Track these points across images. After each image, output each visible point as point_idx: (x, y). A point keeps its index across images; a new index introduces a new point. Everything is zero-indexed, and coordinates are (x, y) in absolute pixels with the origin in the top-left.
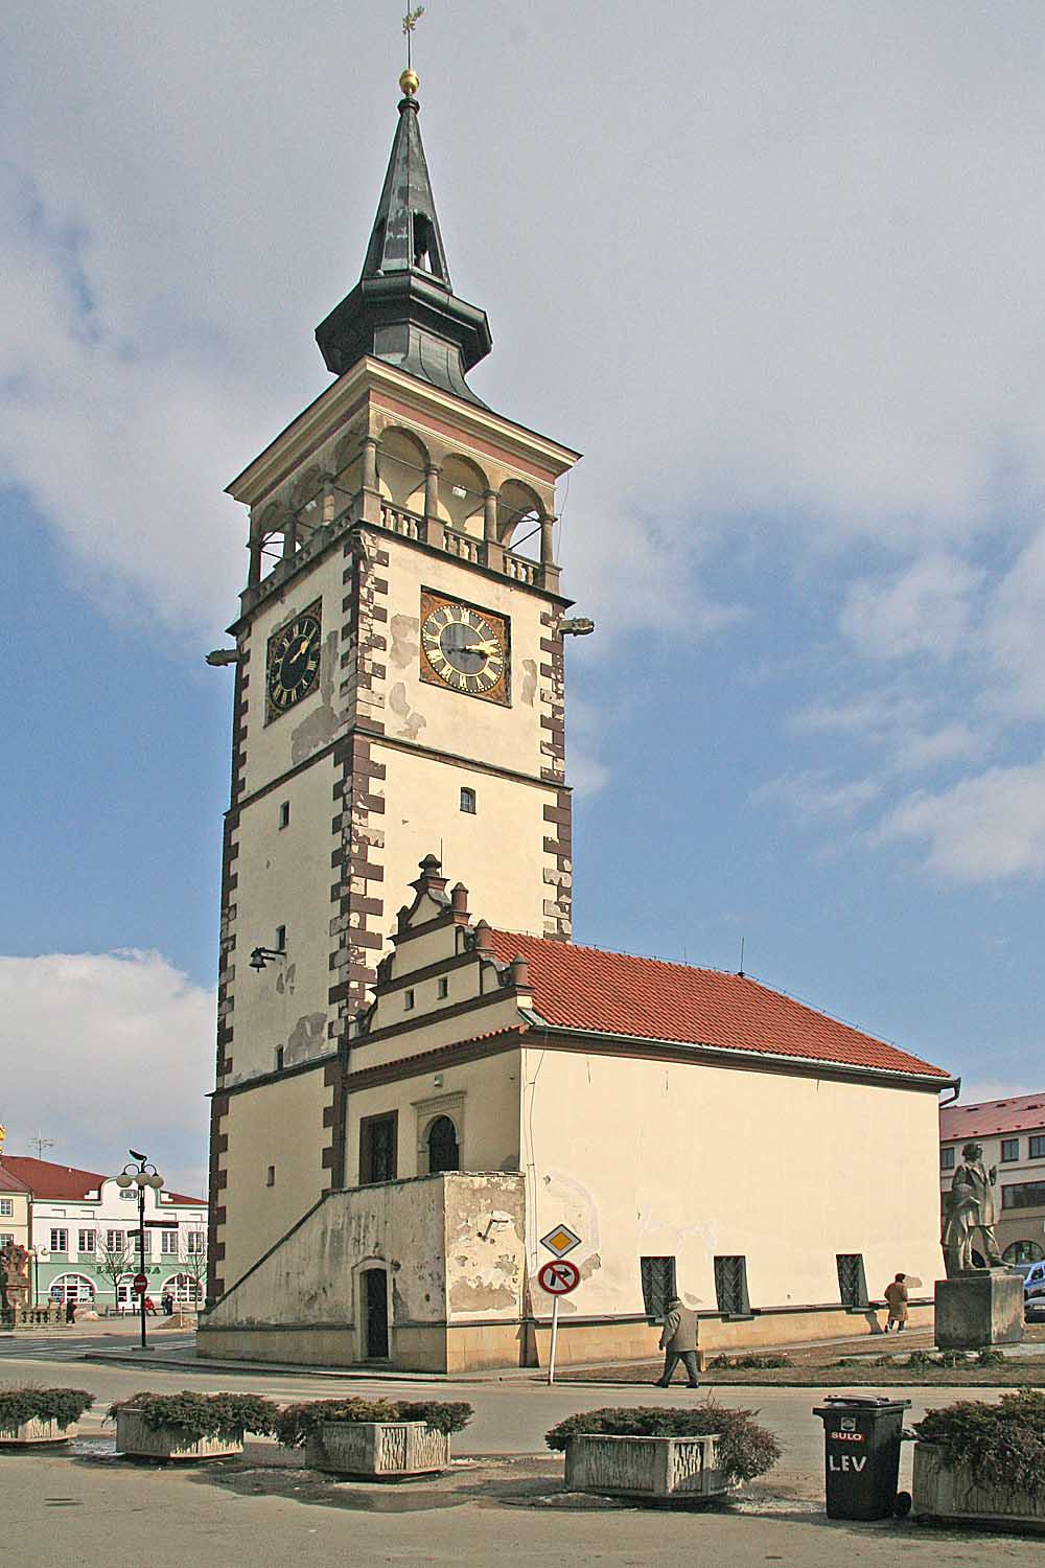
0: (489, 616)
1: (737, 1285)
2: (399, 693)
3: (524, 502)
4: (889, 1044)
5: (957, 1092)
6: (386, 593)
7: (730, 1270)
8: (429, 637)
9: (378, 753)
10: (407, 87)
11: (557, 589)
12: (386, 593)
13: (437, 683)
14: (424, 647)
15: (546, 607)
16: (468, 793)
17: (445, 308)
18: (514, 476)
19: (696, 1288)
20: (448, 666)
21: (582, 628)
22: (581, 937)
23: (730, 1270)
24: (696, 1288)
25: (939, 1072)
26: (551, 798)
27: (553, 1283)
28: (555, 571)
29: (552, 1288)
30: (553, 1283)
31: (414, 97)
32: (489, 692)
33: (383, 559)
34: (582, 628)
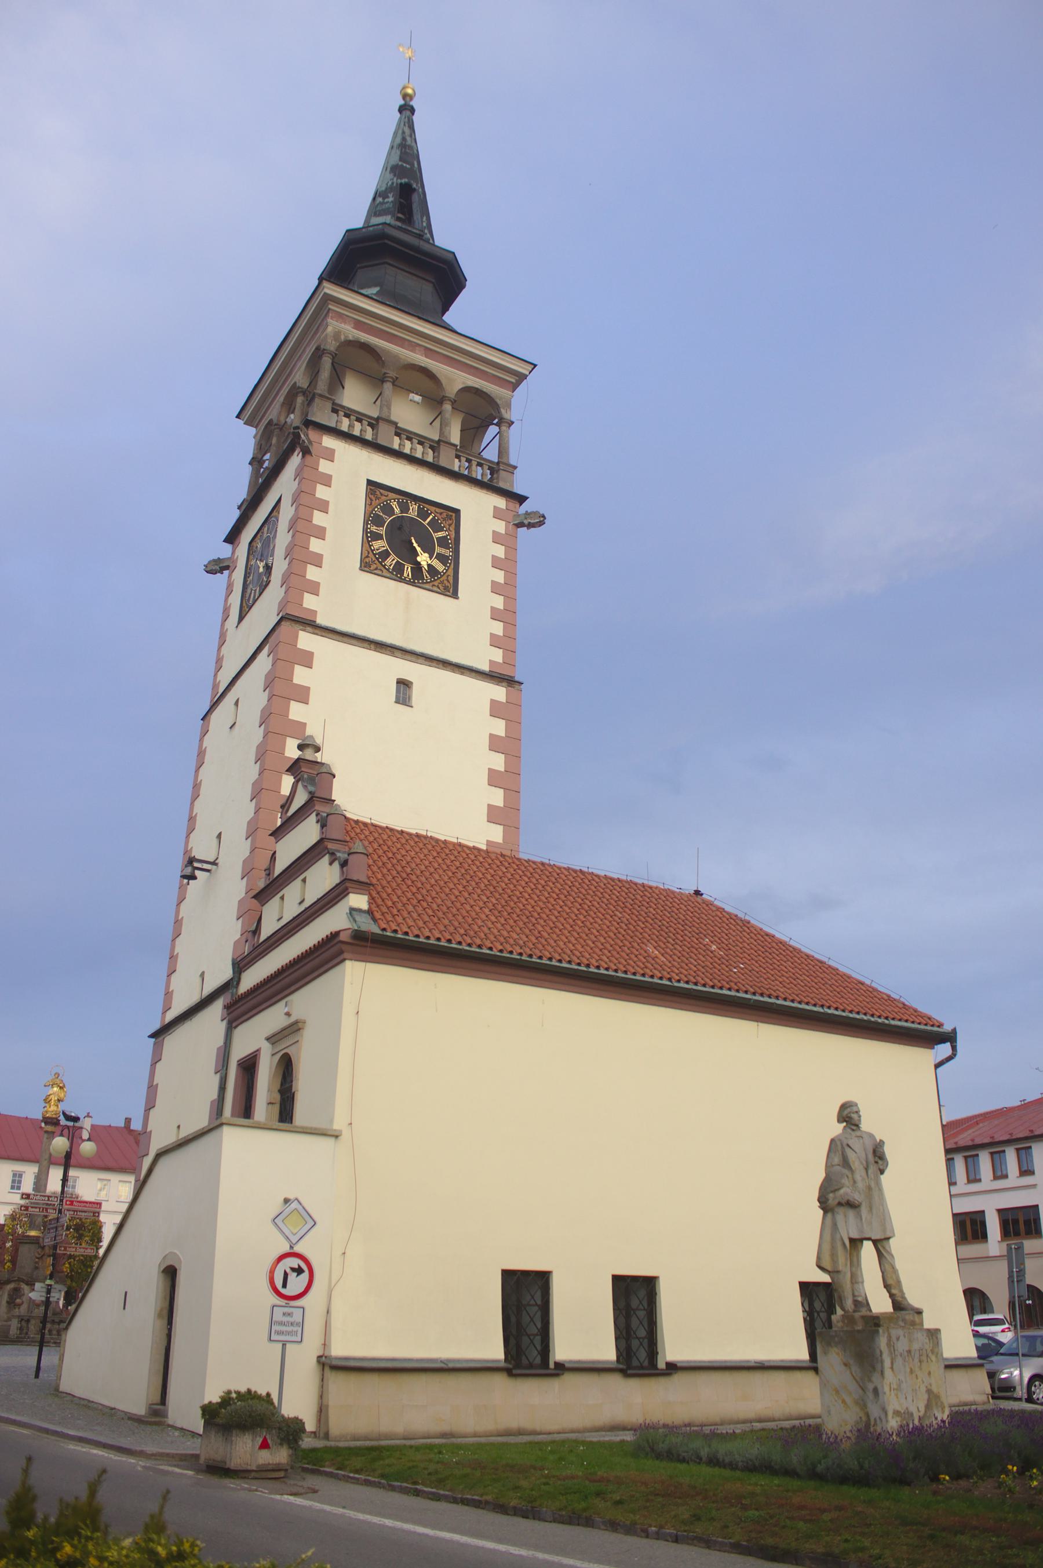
0: (438, 510)
1: (628, 1317)
2: (346, 587)
3: (482, 413)
4: (868, 982)
5: (954, 1048)
6: (370, 483)
7: (635, 1300)
8: (374, 529)
9: (306, 640)
10: (405, 96)
11: (513, 487)
12: (370, 483)
13: (380, 572)
14: (368, 537)
15: (501, 502)
16: (404, 685)
17: (418, 250)
18: (470, 383)
19: (582, 1330)
20: (393, 556)
21: (537, 521)
22: (529, 851)
23: (635, 1300)
24: (582, 1330)
25: (929, 1020)
26: (500, 692)
27: (284, 1285)
28: (511, 469)
29: (283, 1291)
30: (284, 1285)
31: (412, 103)
32: (436, 583)
33: (330, 455)
34: (537, 521)
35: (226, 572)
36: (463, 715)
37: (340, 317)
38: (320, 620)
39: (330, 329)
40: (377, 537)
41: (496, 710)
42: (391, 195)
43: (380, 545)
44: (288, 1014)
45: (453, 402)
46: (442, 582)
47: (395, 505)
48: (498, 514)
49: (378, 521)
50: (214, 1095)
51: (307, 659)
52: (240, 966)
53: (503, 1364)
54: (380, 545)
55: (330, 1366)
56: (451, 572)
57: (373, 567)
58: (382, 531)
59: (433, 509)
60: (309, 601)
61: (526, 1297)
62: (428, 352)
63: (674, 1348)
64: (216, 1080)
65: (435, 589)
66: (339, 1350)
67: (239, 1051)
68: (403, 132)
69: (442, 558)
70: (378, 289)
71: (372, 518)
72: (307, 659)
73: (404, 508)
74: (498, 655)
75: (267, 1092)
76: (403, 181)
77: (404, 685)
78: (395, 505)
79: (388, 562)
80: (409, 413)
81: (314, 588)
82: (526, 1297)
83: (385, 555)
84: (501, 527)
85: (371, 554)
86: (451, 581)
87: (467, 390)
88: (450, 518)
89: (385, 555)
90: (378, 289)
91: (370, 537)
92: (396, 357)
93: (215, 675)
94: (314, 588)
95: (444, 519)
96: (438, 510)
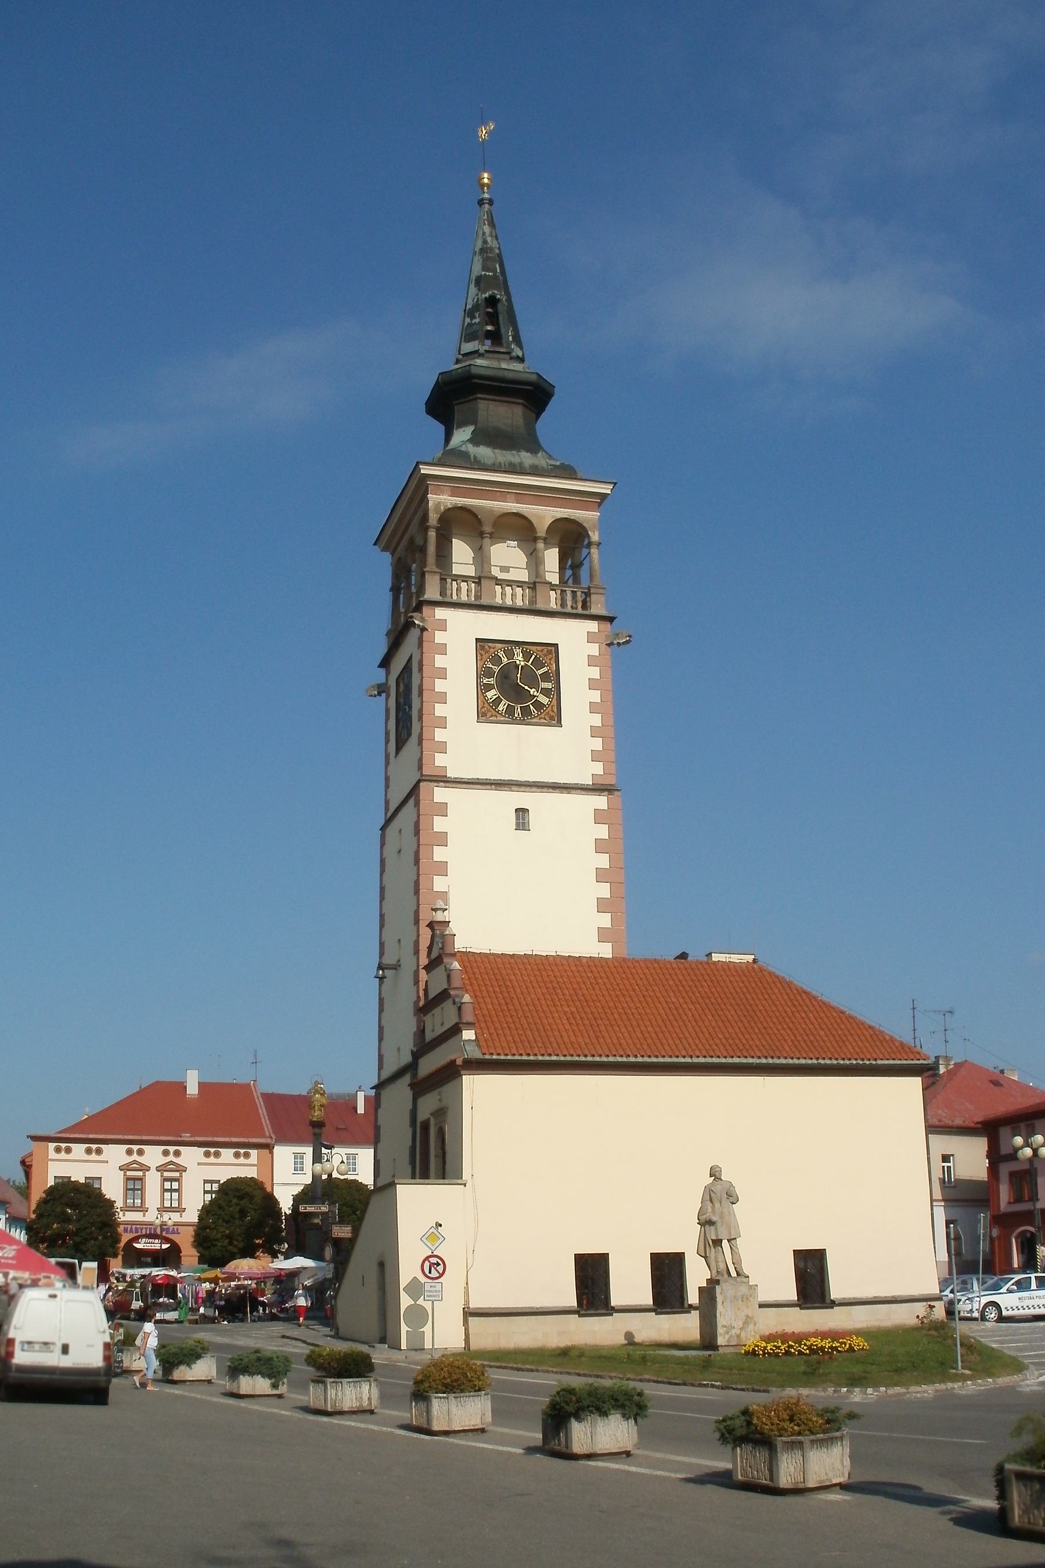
15: (593, 626)
16: (521, 813)
18: (559, 516)
32: (543, 716)
35: (384, 695)
36: (575, 830)
37: (439, 491)
38: (451, 774)
39: (430, 504)
40: (488, 687)
41: (600, 817)
42: (477, 315)
43: (492, 694)
44: (440, 1100)
45: (545, 539)
46: (548, 714)
47: (501, 654)
48: (591, 638)
49: (488, 673)
50: (409, 1143)
51: (442, 810)
52: (416, 1056)
53: (652, 1307)
54: (492, 694)
55: (469, 1313)
56: (554, 702)
57: (489, 715)
58: (496, 669)
59: (534, 648)
60: (440, 760)
61: (592, 1275)
62: (519, 499)
63: (837, 1290)
64: (410, 1131)
65: (543, 721)
66: (474, 1305)
67: (422, 1116)
68: (484, 234)
69: (546, 692)
70: (472, 428)
71: (483, 672)
72: (442, 810)
73: (510, 654)
74: (598, 768)
75: (433, 1154)
76: (487, 295)
77: (521, 813)
78: (501, 654)
79: (500, 708)
80: (507, 557)
81: (442, 747)
82: (592, 1275)
83: (497, 701)
84: (594, 649)
85: (486, 705)
86: (555, 710)
87: (558, 521)
88: (550, 652)
89: (497, 701)
90: (472, 428)
91: (483, 689)
92: (490, 511)
93: (386, 795)
94: (442, 747)
95: (545, 655)
96: (539, 648)
